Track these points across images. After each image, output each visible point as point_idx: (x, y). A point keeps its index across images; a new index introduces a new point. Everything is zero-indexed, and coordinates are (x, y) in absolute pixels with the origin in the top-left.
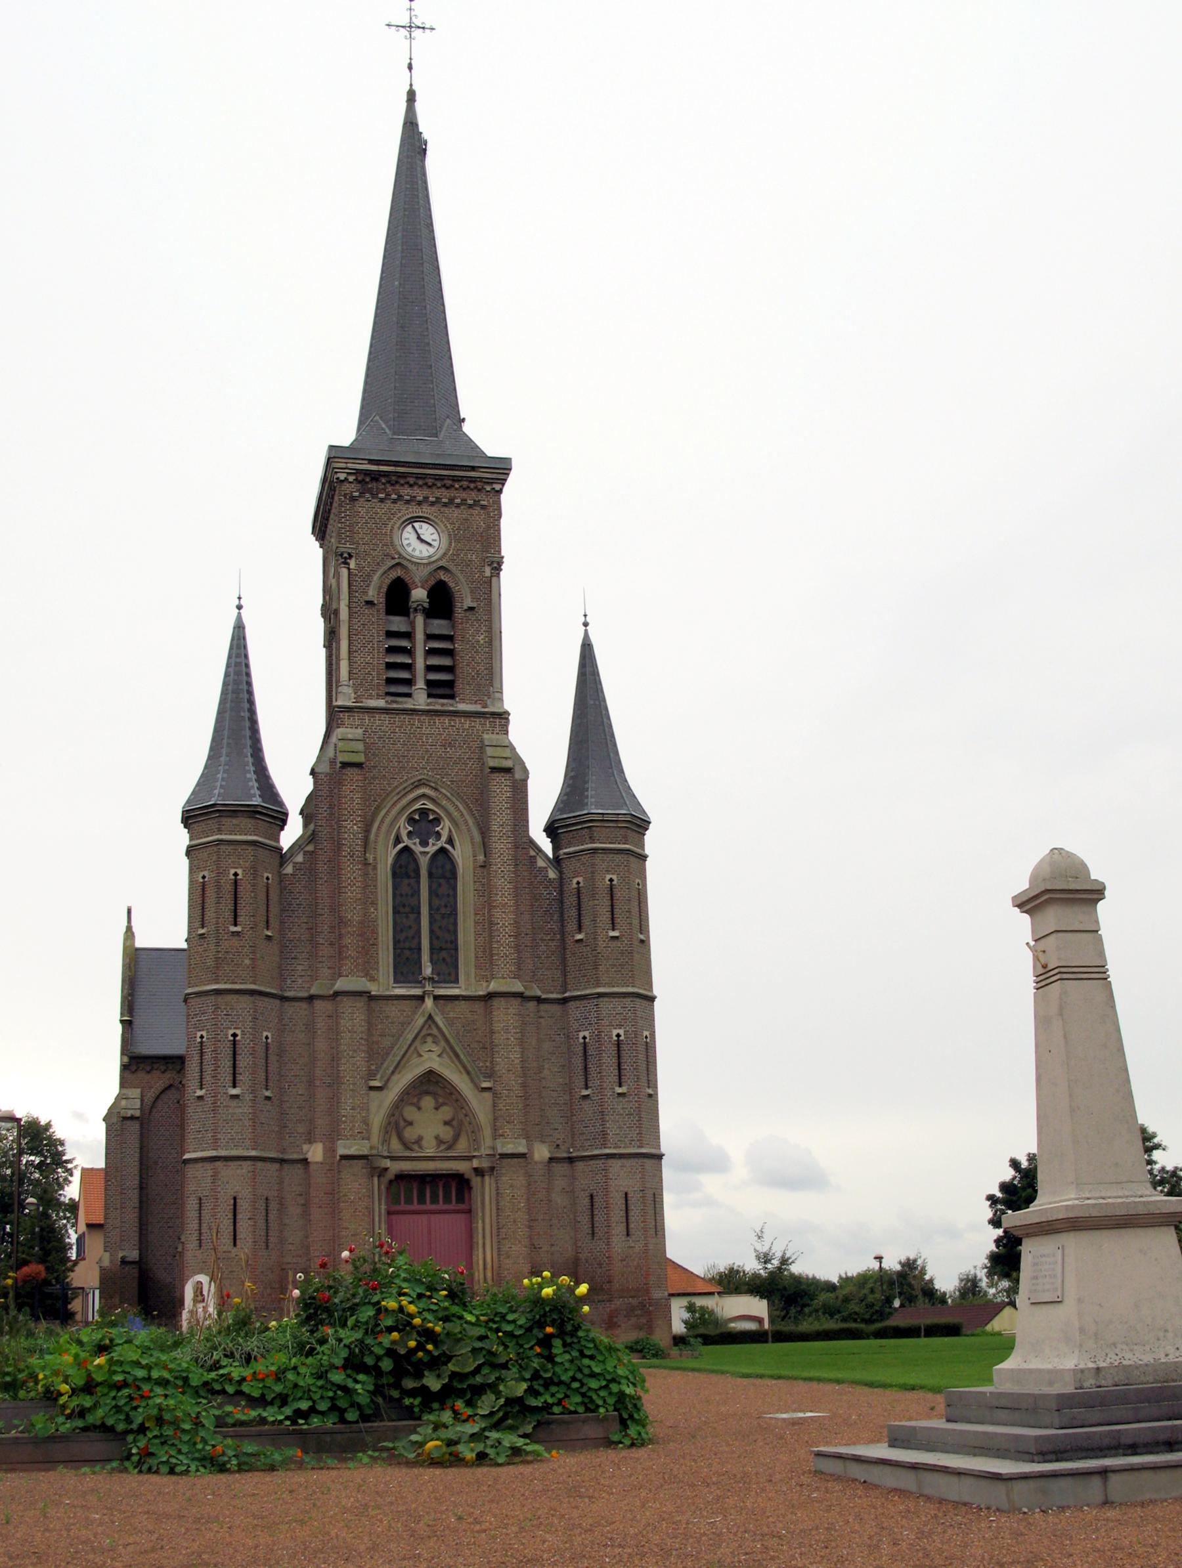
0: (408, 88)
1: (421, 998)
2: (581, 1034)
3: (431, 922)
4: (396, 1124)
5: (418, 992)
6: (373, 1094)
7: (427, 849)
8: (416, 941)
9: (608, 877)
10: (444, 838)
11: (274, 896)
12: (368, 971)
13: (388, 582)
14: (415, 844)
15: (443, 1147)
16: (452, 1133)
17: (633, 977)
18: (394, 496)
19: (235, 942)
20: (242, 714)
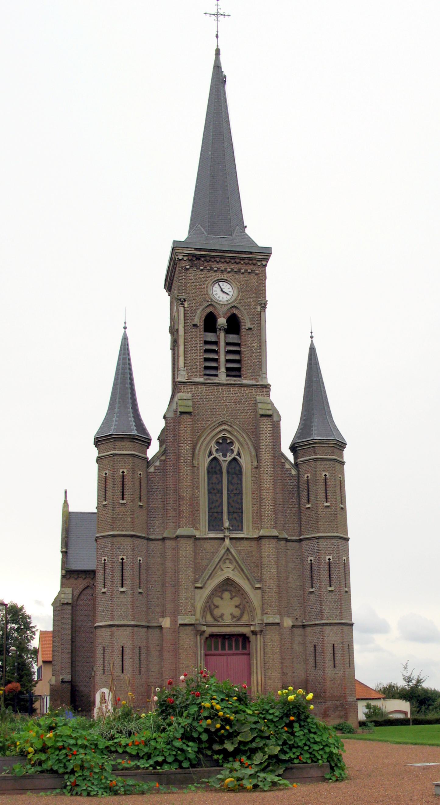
0: (216, 47)
2: (309, 559)
5: (221, 536)
6: (197, 590)
9: (324, 474)
10: (235, 453)
11: (144, 484)
12: (195, 524)
13: (205, 314)
14: (220, 456)
15: (235, 619)
16: (239, 612)
17: (337, 527)
18: (208, 268)
19: (123, 509)
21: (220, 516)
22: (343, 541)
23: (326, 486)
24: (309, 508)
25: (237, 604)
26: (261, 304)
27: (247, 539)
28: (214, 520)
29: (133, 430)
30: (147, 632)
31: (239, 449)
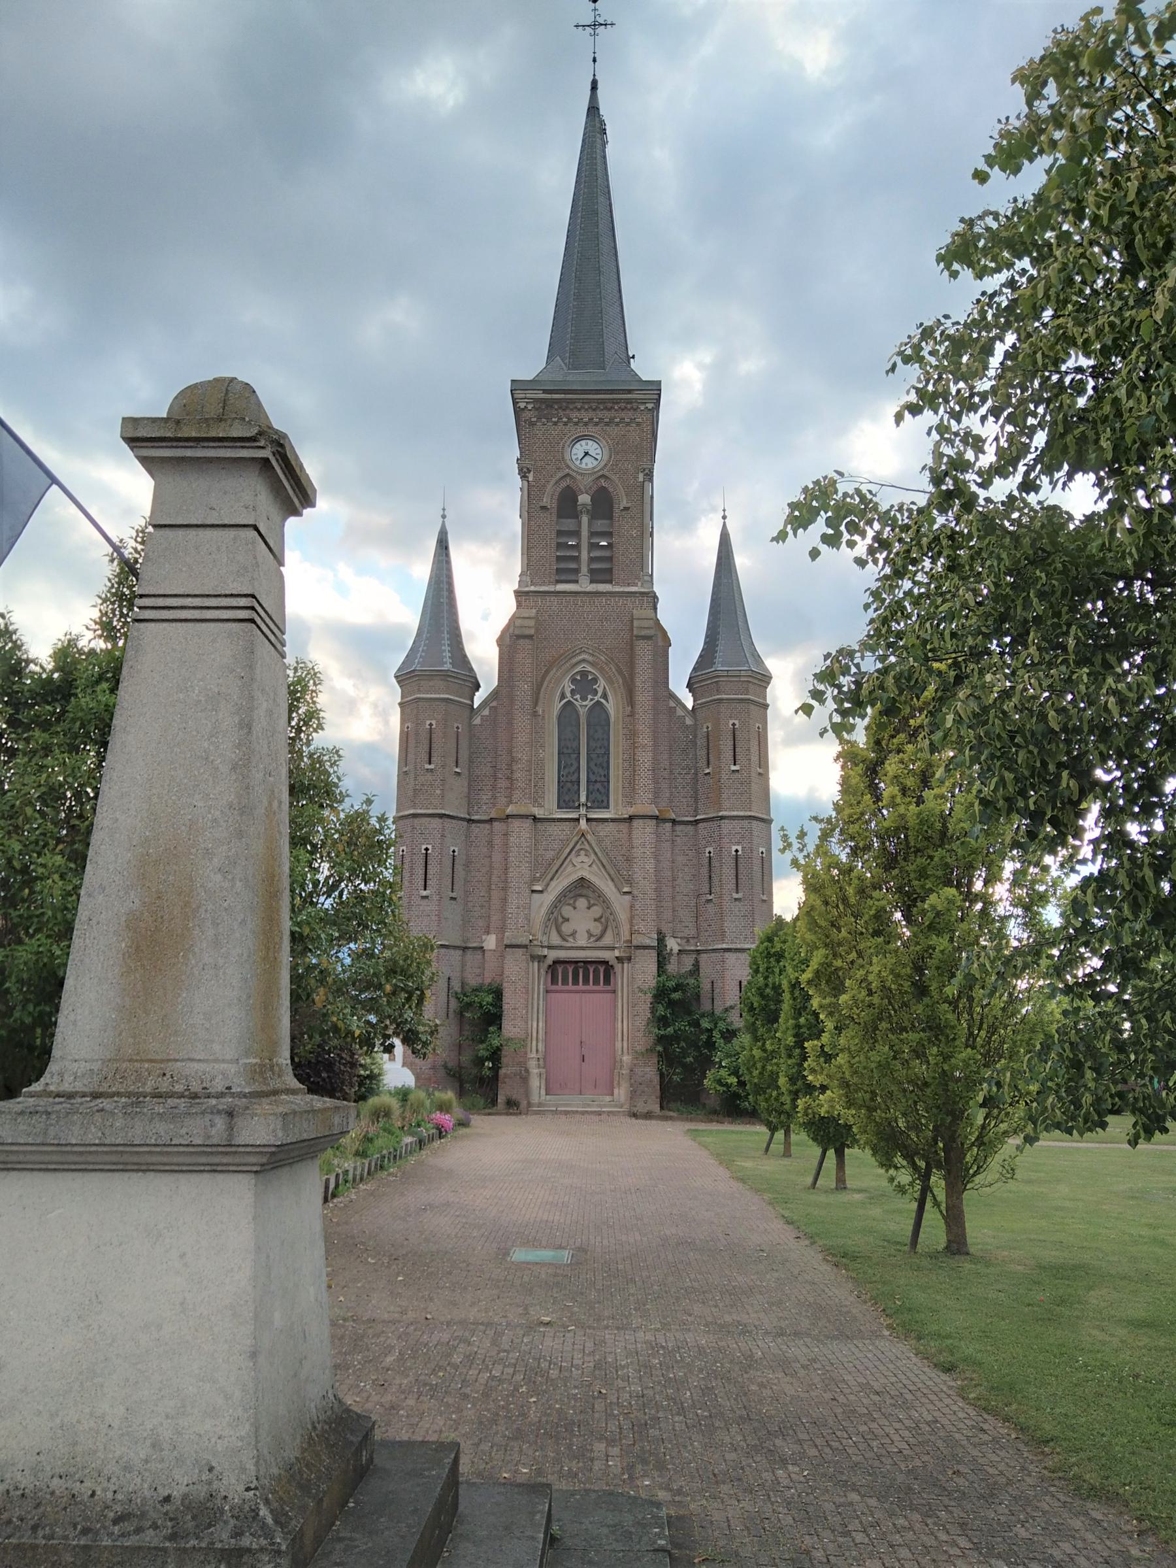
3: (589, 760)
4: (555, 919)
5: (574, 815)
6: (535, 895)
10: (599, 694)
11: (464, 744)
12: (537, 801)
13: (559, 490)
15: (592, 939)
18: (565, 420)
19: (429, 776)
22: (761, 824)
25: (598, 916)
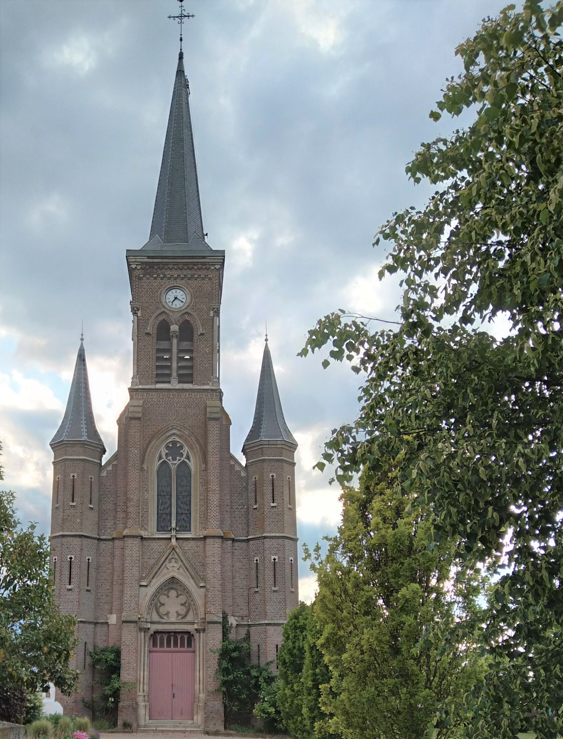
0: (179, 51)
1: (170, 539)
2: (255, 559)
5: (168, 536)
6: (142, 588)
7: (174, 462)
8: (169, 509)
9: (271, 475)
10: (184, 456)
13: (158, 322)
14: (169, 460)
15: (180, 617)
16: (185, 610)
17: (284, 528)
18: (162, 276)
19: (72, 510)
20: (81, 394)
21: (169, 517)
23: (273, 487)
24: (256, 508)
25: (183, 602)
26: (214, 309)
27: (193, 539)
28: (163, 521)
29: (84, 436)
30: (95, 628)
31: (188, 452)
